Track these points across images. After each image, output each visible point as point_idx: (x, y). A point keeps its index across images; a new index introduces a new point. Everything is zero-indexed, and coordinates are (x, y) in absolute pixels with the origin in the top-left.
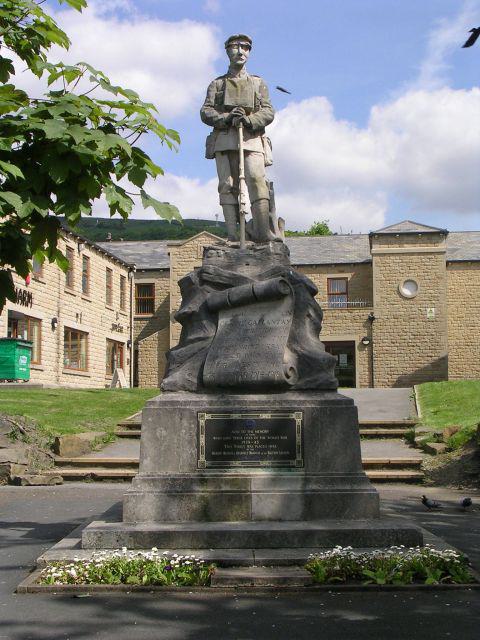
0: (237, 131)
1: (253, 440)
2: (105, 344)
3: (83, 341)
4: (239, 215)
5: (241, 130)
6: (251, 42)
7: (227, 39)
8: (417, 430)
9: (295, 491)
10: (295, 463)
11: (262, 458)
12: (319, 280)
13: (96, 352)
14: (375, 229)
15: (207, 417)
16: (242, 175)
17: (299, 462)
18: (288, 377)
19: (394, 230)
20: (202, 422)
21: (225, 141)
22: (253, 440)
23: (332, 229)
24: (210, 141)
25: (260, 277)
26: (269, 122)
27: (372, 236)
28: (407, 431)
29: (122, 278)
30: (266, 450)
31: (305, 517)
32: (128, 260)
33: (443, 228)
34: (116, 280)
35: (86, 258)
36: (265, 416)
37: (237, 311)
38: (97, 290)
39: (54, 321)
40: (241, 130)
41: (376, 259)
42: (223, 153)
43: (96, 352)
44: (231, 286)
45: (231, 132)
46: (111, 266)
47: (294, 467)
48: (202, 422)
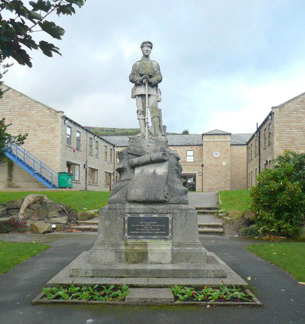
0: (145, 85)
1: (149, 227)
2: (104, 174)
3: (96, 172)
4: (146, 124)
5: (147, 85)
6: (152, 45)
7: (141, 43)
8: (220, 211)
9: (168, 250)
10: (168, 237)
11: (154, 235)
12: (124, 262)
13: (101, 177)
14: (204, 132)
15: (129, 216)
16: (147, 106)
17: (170, 237)
18: (166, 198)
19: (211, 133)
20: (126, 218)
21: (141, 90)
22: (149, 227)
23: (189, 133)
24: (133, 90)
25: (155, 151)
26: (160, 81)
27: (203, 135)
28: (216, 211)
29: (111, 149)
30: (155, 231)
31: (172, 262)
32: (114, 143)
33: (230, 132)
34: (109, 150)
35: (97, 142)
36: (155, 216)
37: (144, 167)
38: (101, 155)
39: (85, 165)
40: (147, 85)
41: (204, 143)
42: (139, 96)
43: (101, 177)
44: (140, 156)
45: (143, 86)
46: (107, 145)
47: (168, 239)
48: (126, 218)
